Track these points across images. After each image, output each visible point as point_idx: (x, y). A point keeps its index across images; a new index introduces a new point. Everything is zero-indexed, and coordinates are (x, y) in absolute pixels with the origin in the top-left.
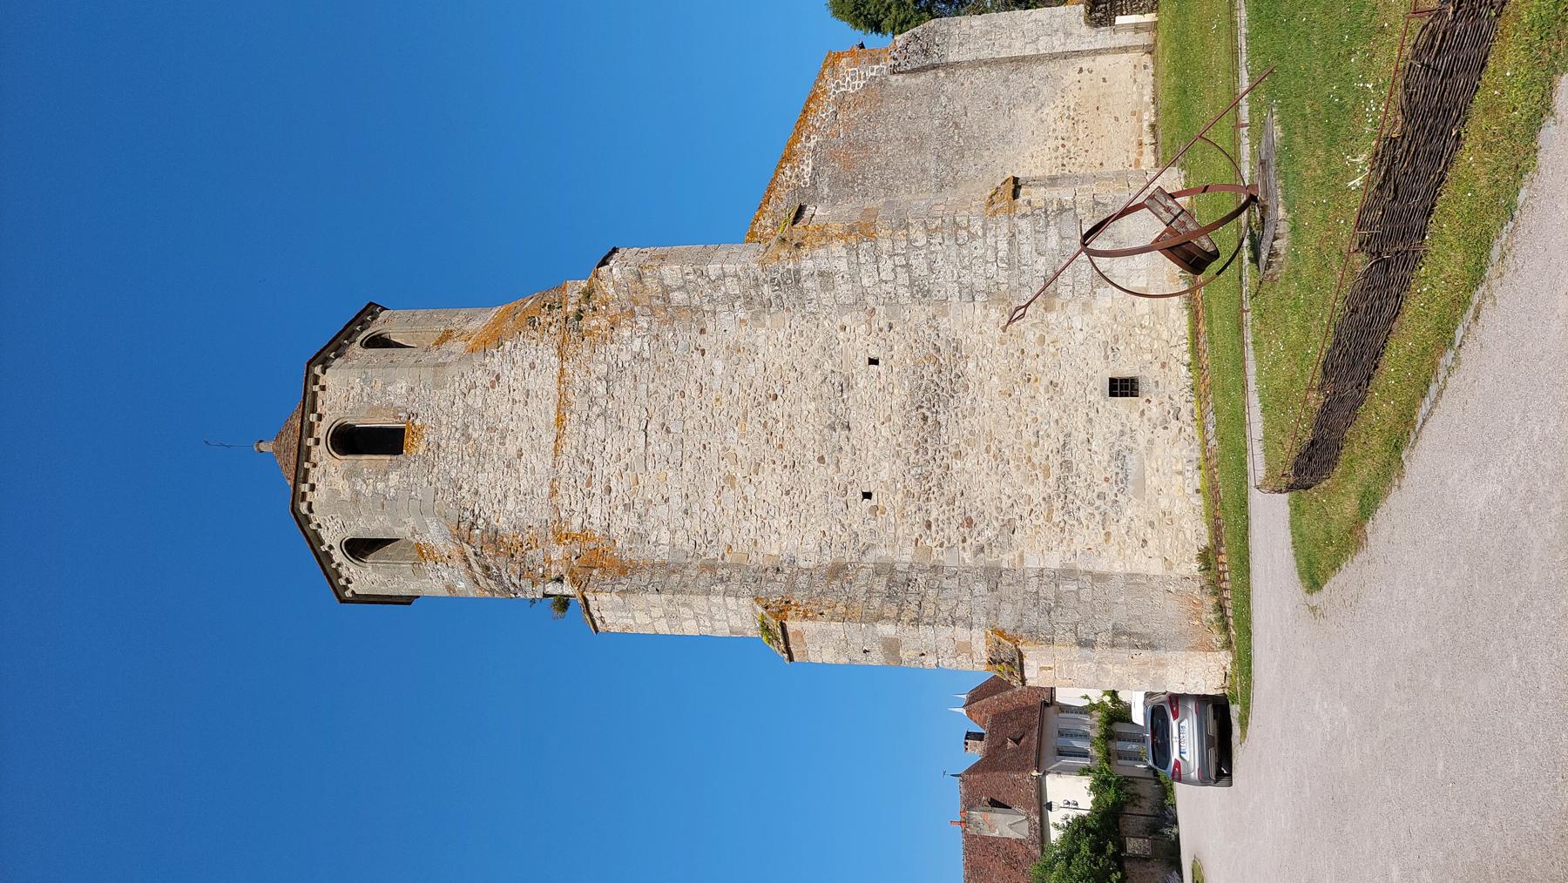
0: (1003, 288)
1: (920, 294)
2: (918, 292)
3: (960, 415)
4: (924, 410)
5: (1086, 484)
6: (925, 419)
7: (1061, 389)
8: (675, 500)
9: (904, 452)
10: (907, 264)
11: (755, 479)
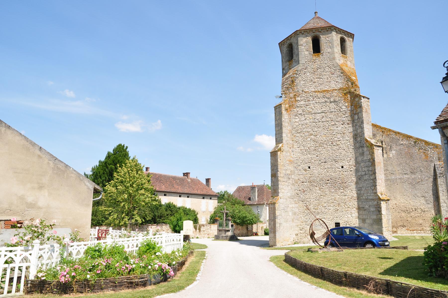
0: (361, 198)
6: (328, 180)
8: (305, 122)
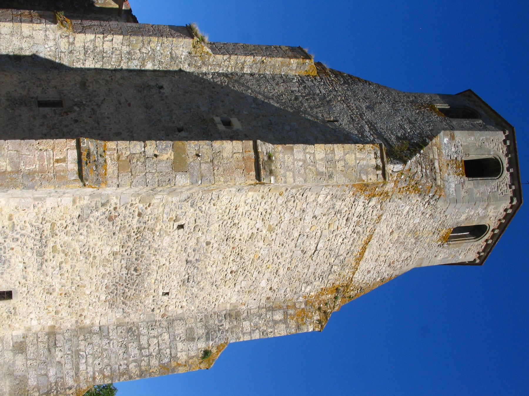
0: (82, 337)
1: (133, 330)
2: (135, 330)
3: (112, 274)
4: (135, 274)
5: (27, 245)
6: (136, 270)
7: (44, 291)
9: (152, 252)
10: (141, 351)
11: (255, 231)
